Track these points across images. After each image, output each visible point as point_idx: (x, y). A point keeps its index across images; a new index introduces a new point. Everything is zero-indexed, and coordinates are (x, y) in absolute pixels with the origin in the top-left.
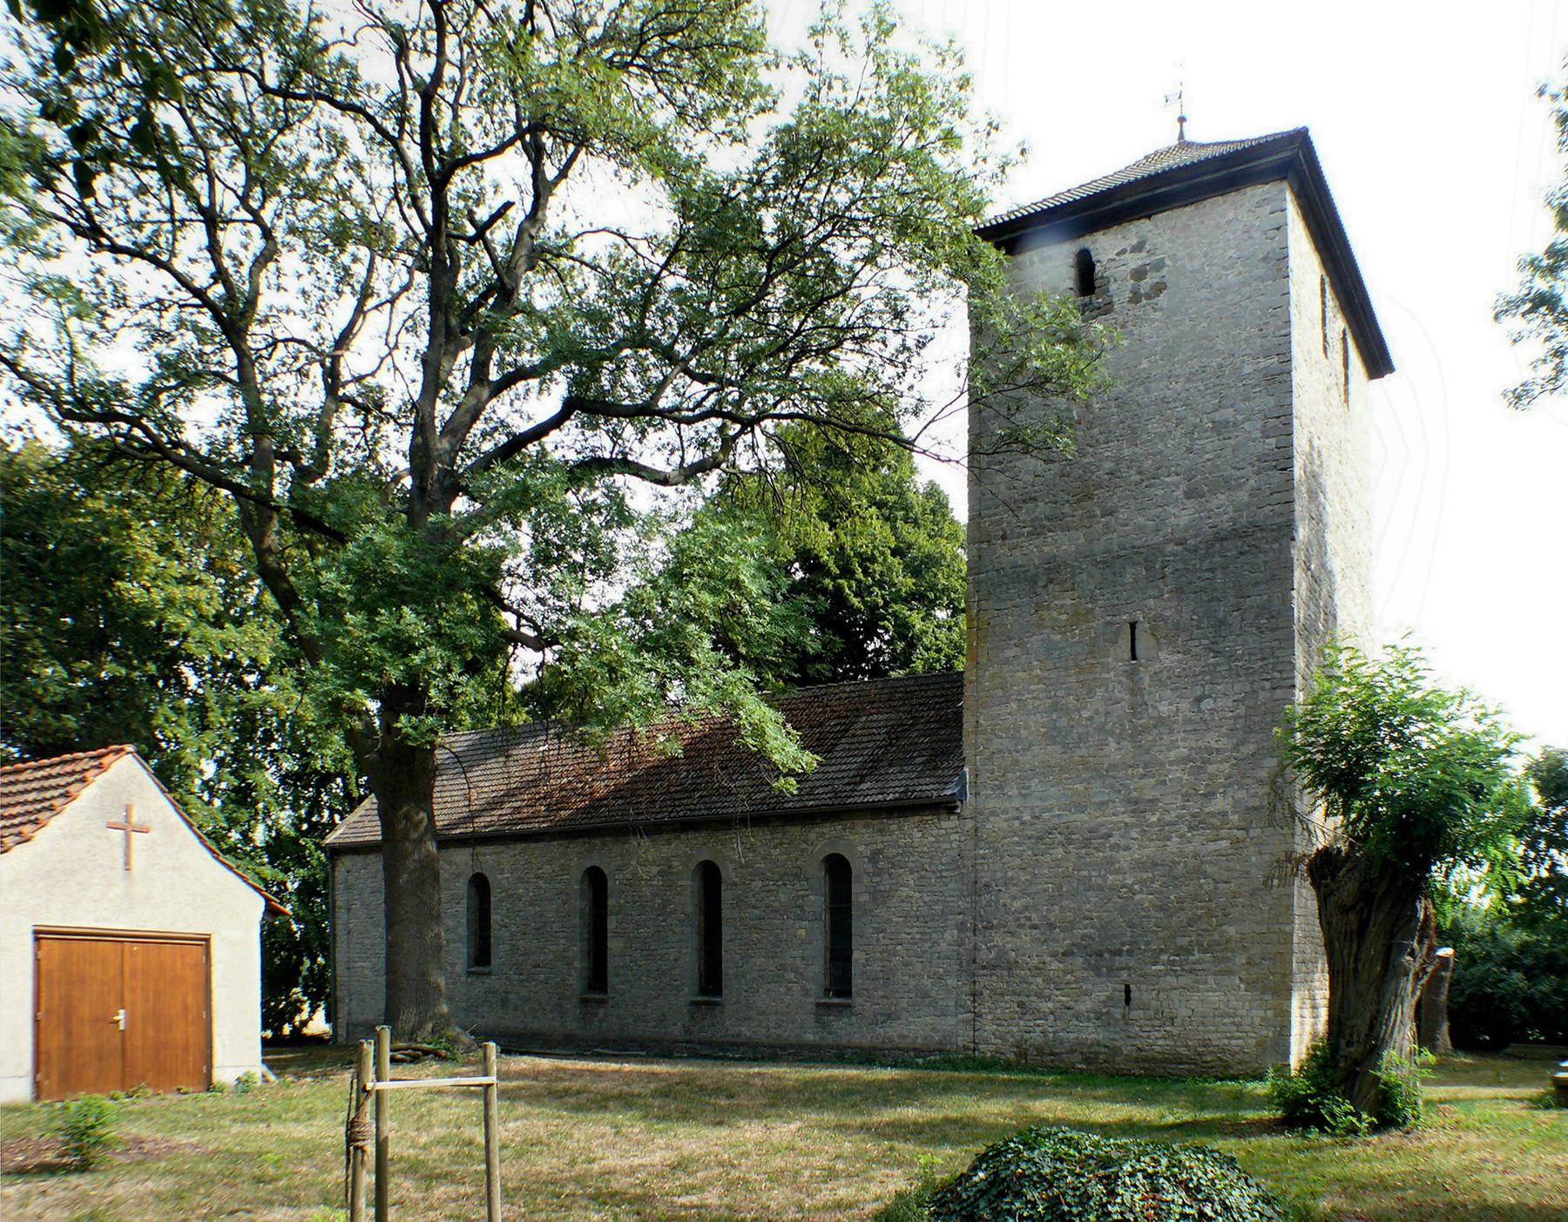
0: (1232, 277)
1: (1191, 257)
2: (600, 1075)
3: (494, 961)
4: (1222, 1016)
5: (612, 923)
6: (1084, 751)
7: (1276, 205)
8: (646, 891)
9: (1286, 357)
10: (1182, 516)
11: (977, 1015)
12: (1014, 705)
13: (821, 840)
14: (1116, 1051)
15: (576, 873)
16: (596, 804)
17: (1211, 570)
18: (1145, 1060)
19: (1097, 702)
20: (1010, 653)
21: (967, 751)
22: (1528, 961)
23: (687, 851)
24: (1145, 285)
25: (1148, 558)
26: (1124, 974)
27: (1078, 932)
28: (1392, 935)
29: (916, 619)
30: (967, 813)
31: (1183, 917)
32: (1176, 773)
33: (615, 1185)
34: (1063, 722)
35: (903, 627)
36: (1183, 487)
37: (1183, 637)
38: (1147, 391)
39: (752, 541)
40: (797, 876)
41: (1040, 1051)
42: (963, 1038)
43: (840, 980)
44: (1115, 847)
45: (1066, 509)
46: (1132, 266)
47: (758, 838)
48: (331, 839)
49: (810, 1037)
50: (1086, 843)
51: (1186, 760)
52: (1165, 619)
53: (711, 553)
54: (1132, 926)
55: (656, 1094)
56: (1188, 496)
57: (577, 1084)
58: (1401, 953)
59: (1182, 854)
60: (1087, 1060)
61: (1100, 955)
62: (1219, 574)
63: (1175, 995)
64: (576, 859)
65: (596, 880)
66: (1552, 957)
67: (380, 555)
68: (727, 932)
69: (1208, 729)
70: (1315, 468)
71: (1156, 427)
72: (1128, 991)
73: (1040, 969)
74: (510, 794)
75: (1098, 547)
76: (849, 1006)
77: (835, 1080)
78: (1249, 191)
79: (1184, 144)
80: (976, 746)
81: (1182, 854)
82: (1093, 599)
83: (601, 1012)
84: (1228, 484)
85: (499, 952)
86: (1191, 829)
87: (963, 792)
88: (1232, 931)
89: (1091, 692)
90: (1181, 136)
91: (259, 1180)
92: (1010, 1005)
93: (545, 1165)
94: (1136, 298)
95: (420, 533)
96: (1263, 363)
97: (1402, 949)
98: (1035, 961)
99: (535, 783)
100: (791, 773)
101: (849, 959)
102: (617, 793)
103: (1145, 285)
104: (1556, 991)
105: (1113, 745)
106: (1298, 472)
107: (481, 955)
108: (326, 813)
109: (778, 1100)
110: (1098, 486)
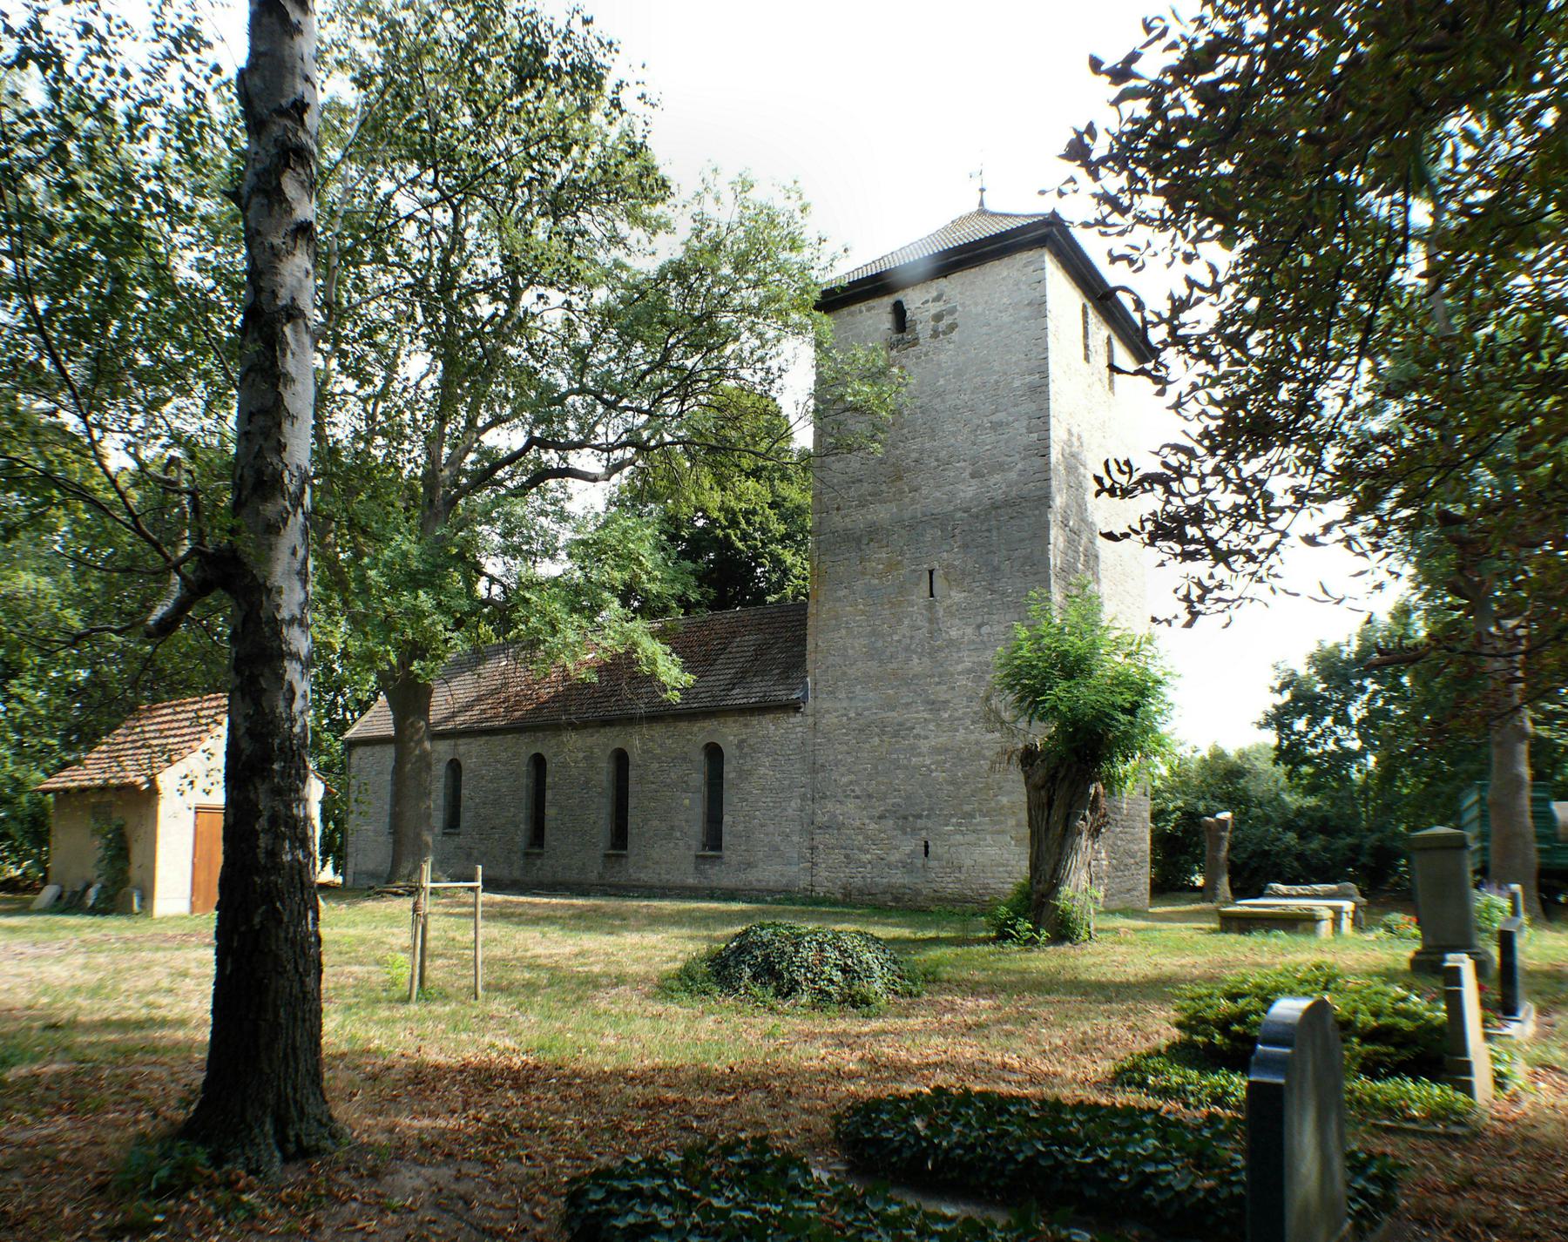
0: (1006, 318)
1: (976, 304)
2: (535, 905)
3: (463, 824)
4: (998, 865)
5: (549, 795)
6: (894, 666)
7: (1037, 265)
8: (574, 772)
9: (1044, 374)
10: (968, 491)
11: (814, 864)
12: (844, 632)
13: (702, 733)
14: (918, 892)
15: (524, 758)
16: (541, 707)
17: (989, 530)
18: (940, 899)
19: (904, 629)
20: (841, 593)
21: (809, 666)
22: (1302, 823)
23: (603, 743)
24: (942, 325)
25: (943, 521)
26: (924, 833)
27: (890, 801)
28: (1070, 806)
29: (788, 558)
30: (808, 712)
31: (968, 789)
32: (963, 681)
33: (539, 961)
34: (880, 644)
35: (777, 561)
36: (968, 471)
37: (968, 580)
38: (943, 401)
39: (648, 532)
40: (684, 759)
41: (861, 892)
42: (804, 882)
43: (713, 838)
44: (917, 737)
45: (884, 487)
46: (933, 312)
47: (658, 730)
48: (348, 734)
49: (691, 881)
50: (896, 735)
51: (969, 671)
52: (955, 567)
53: (620, 542)
54: (930, 796)
55: (572, 917)
56: (973, 476)
57: (519, 910)
58: (1076, 817)
59: (967, 742)
60: (896, 899)
61: (905, 818)
62: (995, 533)
63: (962, 849)
64: (524, 748)
65: (539, 762)
66: (1325, 819)
67: (405, 555)
68: (632, 802)
69: (986, 648)
70: (1074, 449)
71: (949, 427)
72: (927, 847)
73: (861, 829)
74: (479, 699)
75: (907, 515)
76: (720, 857)
77: (699, 909)
78: (1018, 256)
79: (982, 212)
80: (816, 662)
81: (967, 742)
82: (902, 553)
83: (538, 862)
84: (1001, 467)
85: (466, 817)
86: (973, 722)
87: (806, 696)
88: (1004, 800)
89: (900, 621)
90: (981, 203)
91: (340, 953)
92: (838, 856)
93: (498, 952)
94: (935, 334)
95: (430, 539)
96: (1028, 379)
97: (1076, 816)
98: (858, 823)
99: (496, 691)
100: (674, 688)
101: (720, 822)
102: (556, 697)
103: (942, 325)
104: (1325, 849)
105: (916, 661)
106: (1055, 455)
107: (453, 820)
108: (340, 711)
109: (656, 921)
110: (908, 470)
